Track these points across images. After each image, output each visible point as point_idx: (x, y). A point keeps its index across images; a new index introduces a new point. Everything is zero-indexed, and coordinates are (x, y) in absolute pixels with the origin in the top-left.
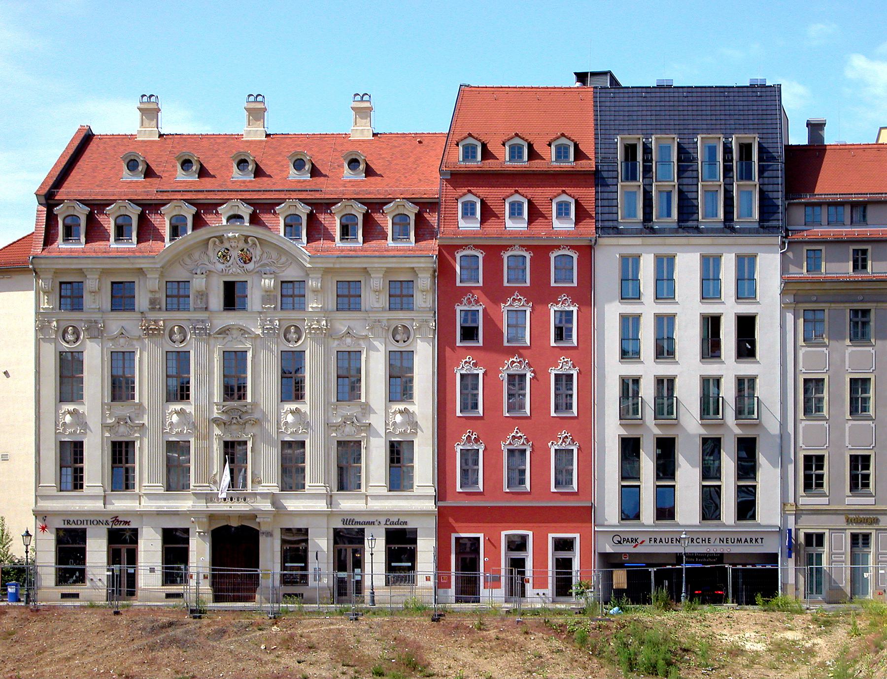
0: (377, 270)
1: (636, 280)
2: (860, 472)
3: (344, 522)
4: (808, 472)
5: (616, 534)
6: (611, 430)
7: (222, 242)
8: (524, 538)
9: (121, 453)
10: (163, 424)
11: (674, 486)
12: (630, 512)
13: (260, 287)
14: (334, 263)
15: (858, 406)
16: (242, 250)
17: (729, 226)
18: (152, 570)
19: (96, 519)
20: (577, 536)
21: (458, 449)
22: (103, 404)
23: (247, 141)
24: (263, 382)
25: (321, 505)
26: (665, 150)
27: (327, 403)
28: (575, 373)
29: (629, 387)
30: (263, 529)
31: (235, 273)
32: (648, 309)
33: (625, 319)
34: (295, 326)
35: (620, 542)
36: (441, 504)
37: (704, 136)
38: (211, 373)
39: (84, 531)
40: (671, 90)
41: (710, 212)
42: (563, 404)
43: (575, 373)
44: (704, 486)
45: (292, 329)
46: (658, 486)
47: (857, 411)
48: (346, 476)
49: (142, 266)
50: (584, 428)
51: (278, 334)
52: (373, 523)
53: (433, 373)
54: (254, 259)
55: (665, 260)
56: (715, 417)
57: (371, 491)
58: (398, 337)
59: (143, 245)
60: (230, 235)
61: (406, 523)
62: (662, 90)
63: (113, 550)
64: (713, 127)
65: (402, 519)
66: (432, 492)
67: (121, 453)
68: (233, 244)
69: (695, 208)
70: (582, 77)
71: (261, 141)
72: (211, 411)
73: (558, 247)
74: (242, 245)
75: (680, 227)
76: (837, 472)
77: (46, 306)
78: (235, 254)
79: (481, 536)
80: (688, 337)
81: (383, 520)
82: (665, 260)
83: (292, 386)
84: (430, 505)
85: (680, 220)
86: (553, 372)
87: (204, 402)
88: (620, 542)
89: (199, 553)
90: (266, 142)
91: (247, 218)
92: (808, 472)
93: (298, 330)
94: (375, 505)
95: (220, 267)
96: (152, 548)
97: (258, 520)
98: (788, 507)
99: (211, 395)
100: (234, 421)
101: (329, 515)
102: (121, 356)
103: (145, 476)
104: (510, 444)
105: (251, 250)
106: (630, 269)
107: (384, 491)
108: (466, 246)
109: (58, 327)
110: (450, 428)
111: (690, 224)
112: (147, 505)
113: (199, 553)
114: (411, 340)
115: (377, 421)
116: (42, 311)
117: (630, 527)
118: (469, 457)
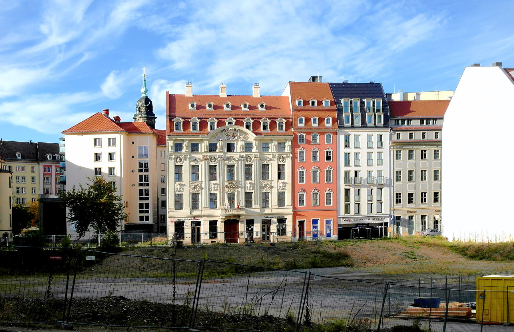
0: (275, 140)
2: (411, 198)
9: (195, 198)
10: (209, 188)
13: (239, 146)
18: (206, 234)
19: (187, 218)
24: (239, 174)
25: (188, 214)
26: (356, 103)
27: (260, 180)
29: (347, 174)
31: (231, 140)
32: (352, 150)
42: (328, 179)
50: (334, 188)
66: (291, 207)
67: (195, 198)
73: (327, 132)
74: (234, 132)
76: (404, 198)
78: (231, 134)
84: (290, 211)
94: (274, 211)
99: (224, 178)
103: (203, 204)
112: (204, 213)
115: (274, 184)
118: (302, 172)
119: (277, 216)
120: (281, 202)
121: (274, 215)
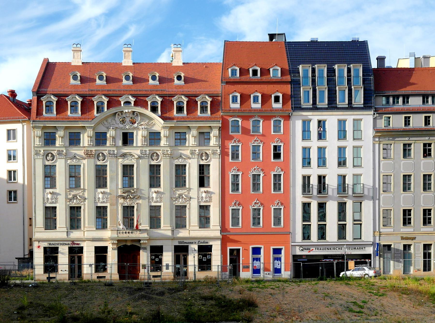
0: (194, 127)
1: (309, 131)
3: (179, 242)
4: (405, 217)
5: (301, 246)
6: (299, 199)
7: (122, 114)
8: (260, 248)
9: (75, 213)
10: (95, 198)
11: (310, 225)
12: (306, 236)
14: (175, 124)
15: (427, 187)
16: (131, 118)
17: (350, 107)
18: (91, 265)
19: (63, 242)
20: (283, 247)
21: (273, 208)
22: (66, 189)
23: (125, 66)
24: (142, 178)
25: (64, 236)
28: (282, 173)
30: (142, 246)
31: (128, 127)
33: (304, 149)
34: (156, 153)
35: (302, 250)
36: (222, 234)
37: (355, 65)
38: (117, 175)
39: (57, 248)
40: (317, 43)
41: (342, 100)
42: (277, 187)
43: (282, 173)
44: (339, 224)
45: (155, 155)
46: (319, 225)
47: (426, 189)
48: (180, 221)
49: (189, 125)
51: (149, 157)
52: (192, 243)
53: (219, 174)
54: (137, 122)
55: (342, 121)
56: (344, 193)
57: (191, 228)
58: (203, 158)
59: (58, 116)
60: (127, 111)
61: (207, 243)
62: (313, 43)
63: (176, 255)
64: (340, 60)
65: (206, 241)
66: (219, 228)
67: (75, 213)
68: (128, 115)
69: (335, 98)
70: (272, 36)
71: (131, 66)
72: (117, 192)
73: (275, 116)
74: (131, 116)
75: (364, 106)
77: (38, 144)
78: (128, 120)
79: (241, 248)
80: (332, 157)
81: (197, 241)
82: (342, 121)
83: (154, 181)
84: (218, 234)
85: (328, 104)
86: (273, 173)
87: (114, 188)
88: (302, 250)
89: (112, 257)
90: (134, 67)
91: (133, 103)
92: (405, 217)
93: (157, 155)
95: (121, 126)
96: (90, 256)
97: (141, 242)
98: (376, 233)
99: (117, 185)
100: (128, 197)
101: (173, 239)
102: (49, 167)
104: (254, 206)
105: (136, 118)
106: (80, 125)
107: (43, 230)
108: (234, 116)
109: (44, 154)
110: (227, 199)
111: (333, 105)
112: (88, 235)
113: (112, 257)
114: (209, 158)
116: (36, 146)
117: (306, 243)
119: (197, 241)
120: (204, 221)
121: (193, 240)
